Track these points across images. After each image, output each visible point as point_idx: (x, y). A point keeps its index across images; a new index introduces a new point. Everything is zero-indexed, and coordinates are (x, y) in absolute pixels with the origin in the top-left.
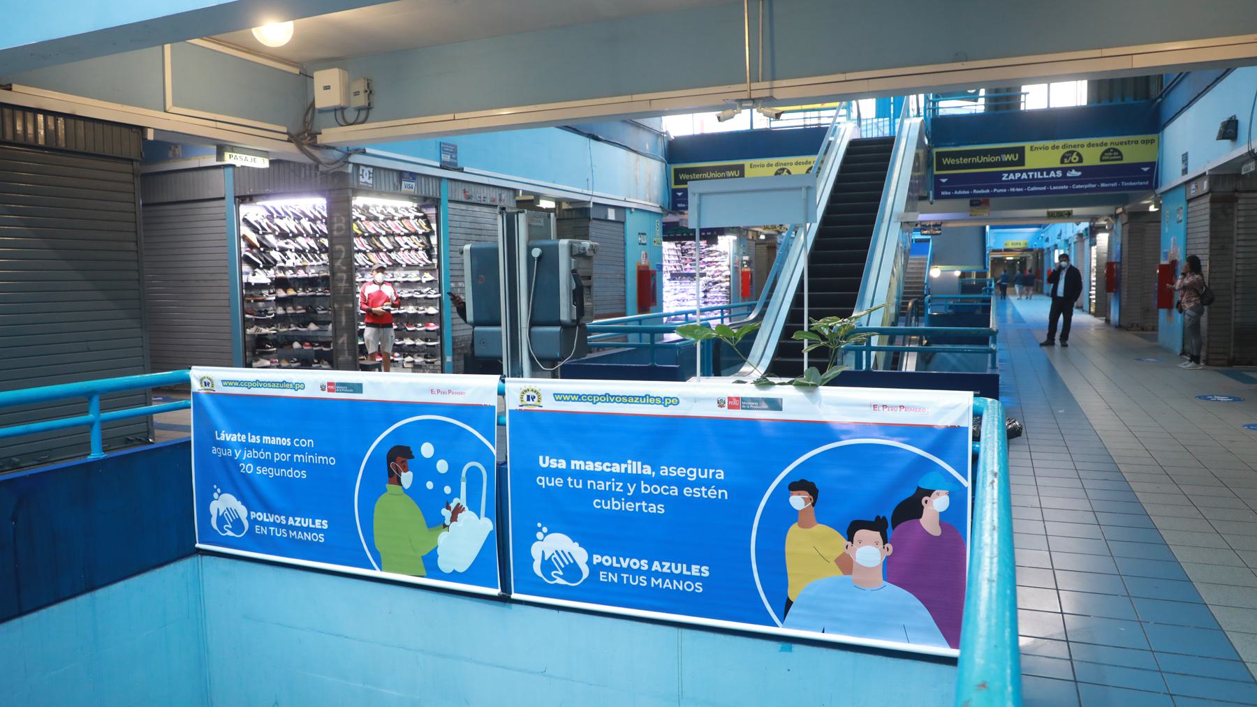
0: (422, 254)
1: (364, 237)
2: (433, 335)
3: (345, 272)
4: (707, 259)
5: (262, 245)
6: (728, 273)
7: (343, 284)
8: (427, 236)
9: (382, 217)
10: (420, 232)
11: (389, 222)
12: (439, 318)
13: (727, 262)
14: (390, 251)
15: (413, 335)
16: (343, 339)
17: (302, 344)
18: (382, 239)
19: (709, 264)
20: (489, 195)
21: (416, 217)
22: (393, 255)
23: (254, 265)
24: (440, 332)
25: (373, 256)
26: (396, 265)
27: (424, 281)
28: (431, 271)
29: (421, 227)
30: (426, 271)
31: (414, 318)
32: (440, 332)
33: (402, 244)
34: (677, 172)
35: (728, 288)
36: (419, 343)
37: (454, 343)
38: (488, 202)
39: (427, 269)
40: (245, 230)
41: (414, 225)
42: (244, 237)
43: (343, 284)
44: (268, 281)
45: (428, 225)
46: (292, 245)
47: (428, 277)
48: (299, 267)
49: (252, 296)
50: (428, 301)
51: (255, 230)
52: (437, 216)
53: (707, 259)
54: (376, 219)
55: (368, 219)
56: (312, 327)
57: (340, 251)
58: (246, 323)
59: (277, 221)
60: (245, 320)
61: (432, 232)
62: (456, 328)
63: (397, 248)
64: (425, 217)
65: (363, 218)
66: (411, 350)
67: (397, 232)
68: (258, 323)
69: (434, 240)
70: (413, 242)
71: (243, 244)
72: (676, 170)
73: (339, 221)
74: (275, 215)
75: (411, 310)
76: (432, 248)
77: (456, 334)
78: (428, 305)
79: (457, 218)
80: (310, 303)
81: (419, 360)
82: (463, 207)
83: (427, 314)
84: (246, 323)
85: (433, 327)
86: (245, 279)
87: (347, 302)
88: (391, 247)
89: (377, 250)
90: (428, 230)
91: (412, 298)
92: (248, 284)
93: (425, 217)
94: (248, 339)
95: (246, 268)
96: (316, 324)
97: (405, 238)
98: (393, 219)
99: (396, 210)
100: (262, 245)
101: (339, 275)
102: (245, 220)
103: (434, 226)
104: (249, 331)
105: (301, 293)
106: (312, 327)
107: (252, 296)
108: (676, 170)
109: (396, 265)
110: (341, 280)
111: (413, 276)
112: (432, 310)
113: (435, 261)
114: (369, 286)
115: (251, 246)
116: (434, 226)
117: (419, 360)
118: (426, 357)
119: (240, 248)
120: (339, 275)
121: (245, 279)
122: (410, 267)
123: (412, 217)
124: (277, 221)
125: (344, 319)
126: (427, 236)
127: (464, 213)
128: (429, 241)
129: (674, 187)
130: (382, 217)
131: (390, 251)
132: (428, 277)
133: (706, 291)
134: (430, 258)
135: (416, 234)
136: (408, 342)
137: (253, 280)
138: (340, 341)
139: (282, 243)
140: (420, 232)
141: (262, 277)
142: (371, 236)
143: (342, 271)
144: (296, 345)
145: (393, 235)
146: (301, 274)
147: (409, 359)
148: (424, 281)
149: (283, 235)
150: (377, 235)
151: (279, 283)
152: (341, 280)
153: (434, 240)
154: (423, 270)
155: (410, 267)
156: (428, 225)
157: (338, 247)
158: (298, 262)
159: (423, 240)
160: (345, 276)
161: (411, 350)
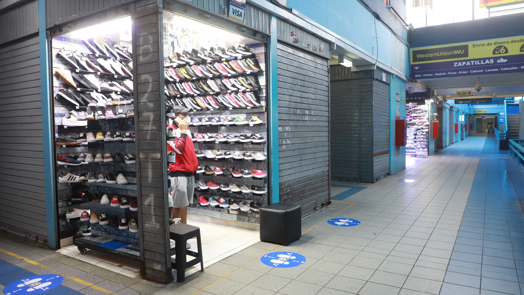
0: (250, 96)
1: (192, 81)
2: (260, 183)
3: (152, 111)
4: (413, 115)
5: (80, 85)
6: (428, 123)
7: (150, 127)
8: (256, 75)
9: (209, 60)
10: (249, 72)
11: (216, 65)
12: (267, 164)
13: (427, 116)
14: (217, 94)
15: (240, 182)
16: (149, 201)
17: (110, 198)
18: (209, 82)
19: (415, 118)
20: (313, 44)
21: (245, 57)
22: (220, 98)
23: (70, 107)
24: (268, 180)
25: (200, 101)
26: (223, 108)
27: (251, 124)
28: (259, 114)
29: (249, 67)
30: (254, 114)
31: (240, 164)
32: (268, 180)
33: (229, 86)
34: (415, 53)
35: (427, 132)
36: (246, 191)
37: (281, 190)
38: (311, 50)
39: (254, 111)
40: (59, 68)
41: (241, 66)
42: (58, 76)
43: (150, 127)
44: (85, 123)
45: (257, 64)
46: (118, 87)
47: (257, 120)
48: (109, 107)
49: (64, 140)
50: (256, 147)
51: (73, 69)
52: (267, 55)
53: (413, 115)
54: (204, 62)
55: (197, 64)
56: (121, 179)
57: (146, 83)
58: (58, 171)
59: (101, 61)
60: (56, 168)
61: (260, 73)
62: (283, 174)
63: (224, 90)
64: (253, 56)
65: (192, 62)
66: (237, 198)
67: (225, 73)
68: (73, 170)
69: (262, 81)
70: (241, 84)
71: (56, 83)
72: (414, 52)
73: (146, 42)
74: (98, 54)
75: (237, 155)
76: (260, 89)
77: (283, 180)
78: (255, 150)
79: (285, 61)
80: (118, 152)
81: (245, 208)
82: (290, 50)
83: (254, 160)
84: (58, 171)
85: (261, 174)
86: (58, 121)
87: (155, 151)
88: (217, 90)
89: (204, 94)
90: (256, 70)
91: (237, 143)
92: (61, 127)
93: (253, 56)
94: (60, 188)
95: (59, 109)
96: (126, 174)
97: (232, 80)
98: (220, 61)
99: (223, 51)
100: (80, 85)
101: (145, 114)
102: (58, 56)
103: (263, 66)
104: (61, 179)
105: (108, 138)
106: (121, 179)
107: (64, 140)
108: (414, 52)
109: (223, 108)
110: (147, 122)
111: (241, 119)
112: (260, 156)
113: (263, 103)
114: (181, 127)
115: (66, 85)
116: (263, 66)
117: (245, 208)
118: (252, 205)
119: (52, 87)
120: (145, 114)
121: (58, 121)
122: (237, 110)
123: (239, 56)
124: (101, 61)
125: (150, 173)
126: (256, 75)
127: (291, 57)
128: (257, 82)
129: (412, 63)
130: (209, 60)
131: (217, 94)
132: (257, 120)
133: (416, 135)
134: (258, 100)
135: (243, 75)
136: (234, 189)
137: (67, 122)
138: (146, 203)
139: (106, 85)
140: (249, 72)
141: (77, 120)
142: (199, 79)
143: (148, 110)
144: (104, 200)
145: (220, 77)
146: (110, 114)
147: (235, 206)
148: (251, 124)
149: (107, 76)
150: (205, 79)
151: (94, 126)
152: (147, 122)
153: (262, 81)
154: (250, 114)
155: (237, 110)
156: (257, 64)
157: (143, 77)
158: (110, 101)
159: (252, 80)
160: (151, 116)
161: (237, 198)
